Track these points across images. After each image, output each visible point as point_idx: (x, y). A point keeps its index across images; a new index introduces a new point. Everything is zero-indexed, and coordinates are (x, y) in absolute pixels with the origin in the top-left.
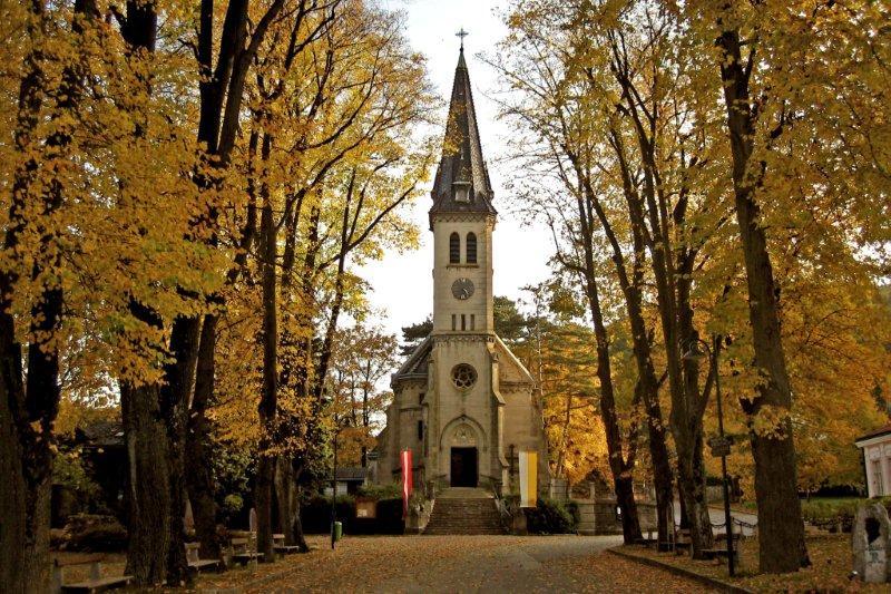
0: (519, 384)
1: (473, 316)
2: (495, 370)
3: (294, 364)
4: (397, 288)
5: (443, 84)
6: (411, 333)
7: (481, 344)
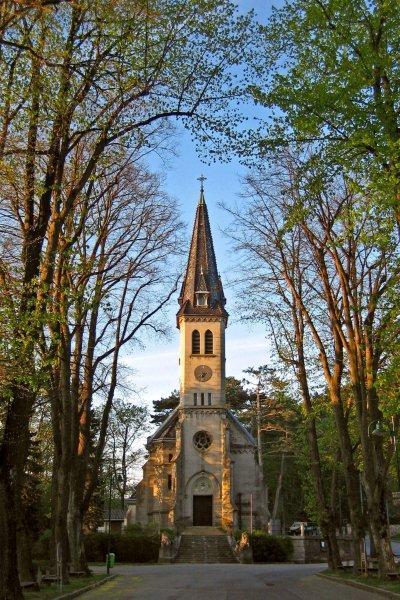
0: (245, 447)
3: (82, 428)
4: (150, 370)
5: (189, 217)
6: (159, 405)
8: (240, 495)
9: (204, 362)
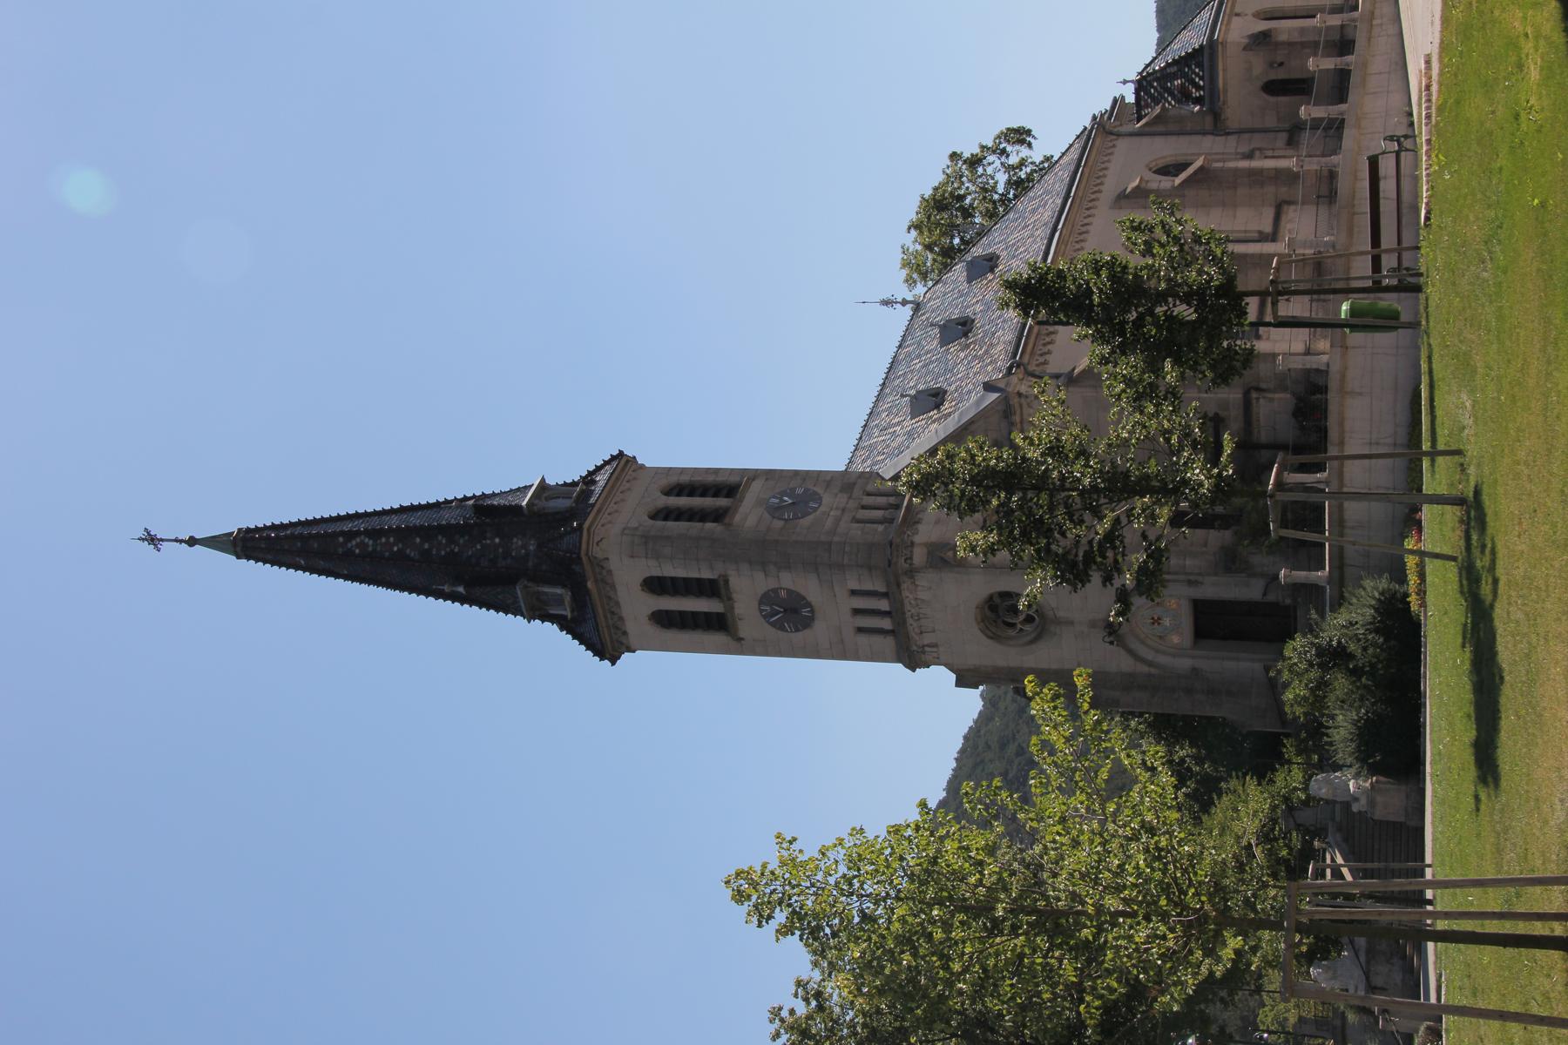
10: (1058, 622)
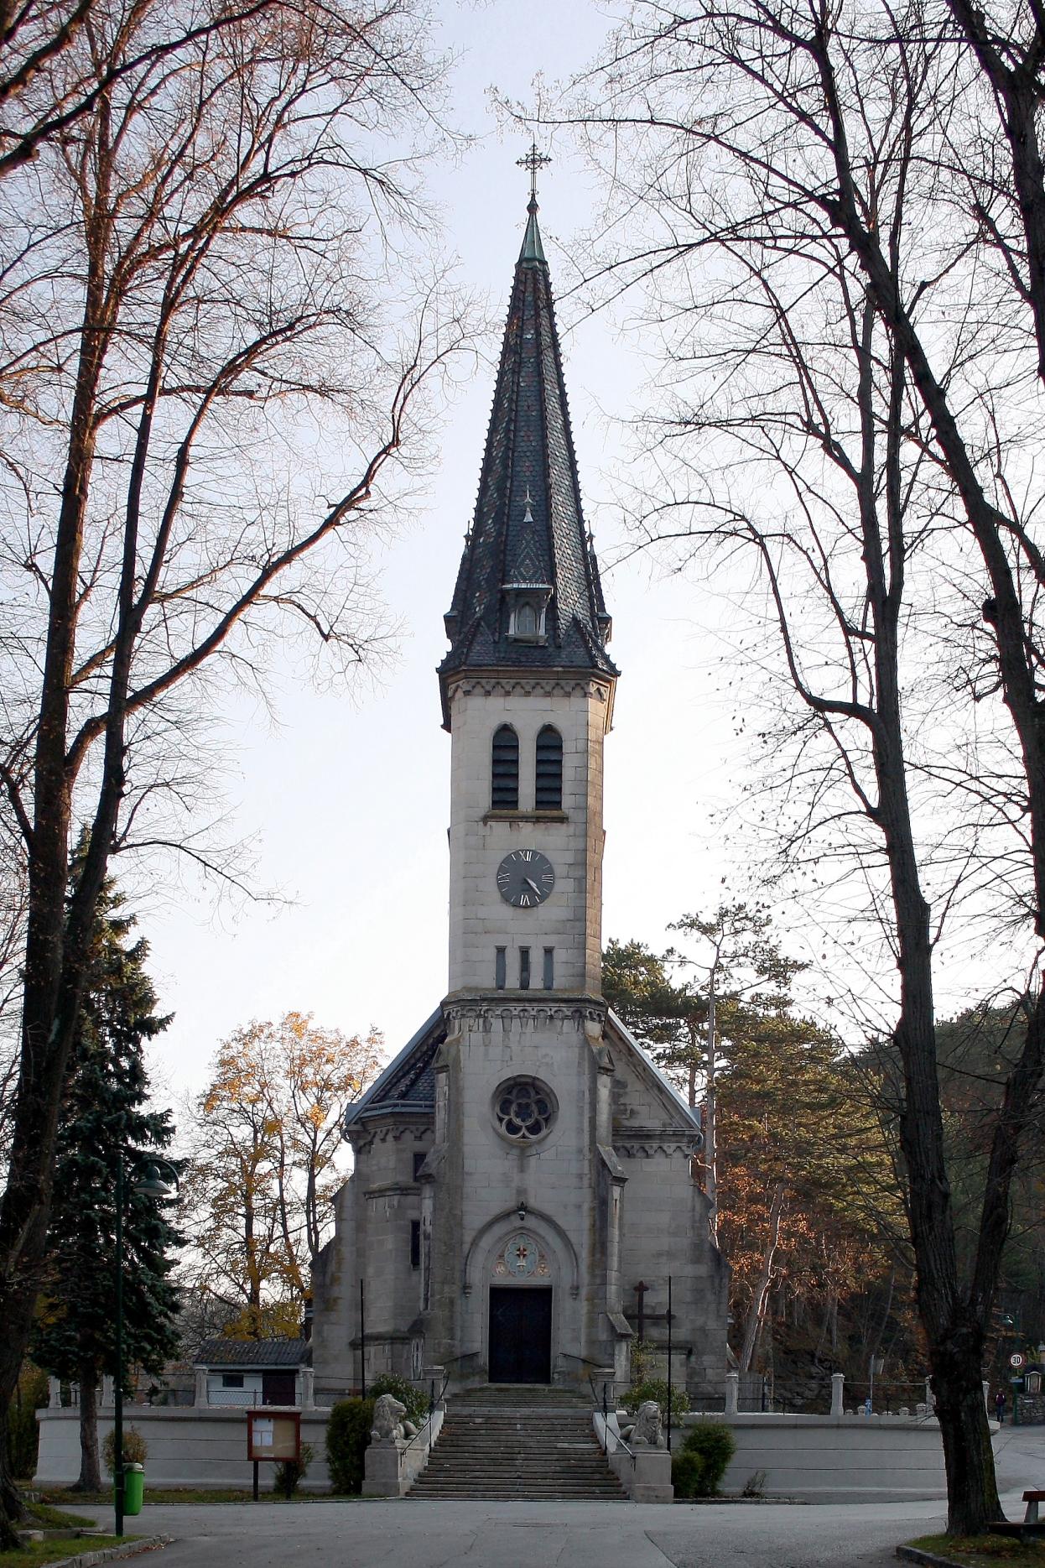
0: (662, 1136)
1: (549, 952)
2: (604, 1093)
7: (568, 1026)
8: (641, 1288)
9: (531, 838)
10: (523, 1152)
